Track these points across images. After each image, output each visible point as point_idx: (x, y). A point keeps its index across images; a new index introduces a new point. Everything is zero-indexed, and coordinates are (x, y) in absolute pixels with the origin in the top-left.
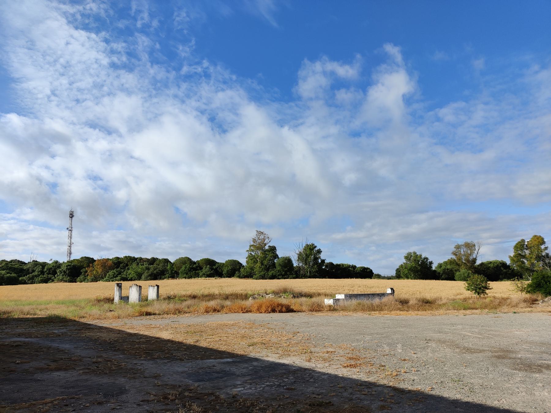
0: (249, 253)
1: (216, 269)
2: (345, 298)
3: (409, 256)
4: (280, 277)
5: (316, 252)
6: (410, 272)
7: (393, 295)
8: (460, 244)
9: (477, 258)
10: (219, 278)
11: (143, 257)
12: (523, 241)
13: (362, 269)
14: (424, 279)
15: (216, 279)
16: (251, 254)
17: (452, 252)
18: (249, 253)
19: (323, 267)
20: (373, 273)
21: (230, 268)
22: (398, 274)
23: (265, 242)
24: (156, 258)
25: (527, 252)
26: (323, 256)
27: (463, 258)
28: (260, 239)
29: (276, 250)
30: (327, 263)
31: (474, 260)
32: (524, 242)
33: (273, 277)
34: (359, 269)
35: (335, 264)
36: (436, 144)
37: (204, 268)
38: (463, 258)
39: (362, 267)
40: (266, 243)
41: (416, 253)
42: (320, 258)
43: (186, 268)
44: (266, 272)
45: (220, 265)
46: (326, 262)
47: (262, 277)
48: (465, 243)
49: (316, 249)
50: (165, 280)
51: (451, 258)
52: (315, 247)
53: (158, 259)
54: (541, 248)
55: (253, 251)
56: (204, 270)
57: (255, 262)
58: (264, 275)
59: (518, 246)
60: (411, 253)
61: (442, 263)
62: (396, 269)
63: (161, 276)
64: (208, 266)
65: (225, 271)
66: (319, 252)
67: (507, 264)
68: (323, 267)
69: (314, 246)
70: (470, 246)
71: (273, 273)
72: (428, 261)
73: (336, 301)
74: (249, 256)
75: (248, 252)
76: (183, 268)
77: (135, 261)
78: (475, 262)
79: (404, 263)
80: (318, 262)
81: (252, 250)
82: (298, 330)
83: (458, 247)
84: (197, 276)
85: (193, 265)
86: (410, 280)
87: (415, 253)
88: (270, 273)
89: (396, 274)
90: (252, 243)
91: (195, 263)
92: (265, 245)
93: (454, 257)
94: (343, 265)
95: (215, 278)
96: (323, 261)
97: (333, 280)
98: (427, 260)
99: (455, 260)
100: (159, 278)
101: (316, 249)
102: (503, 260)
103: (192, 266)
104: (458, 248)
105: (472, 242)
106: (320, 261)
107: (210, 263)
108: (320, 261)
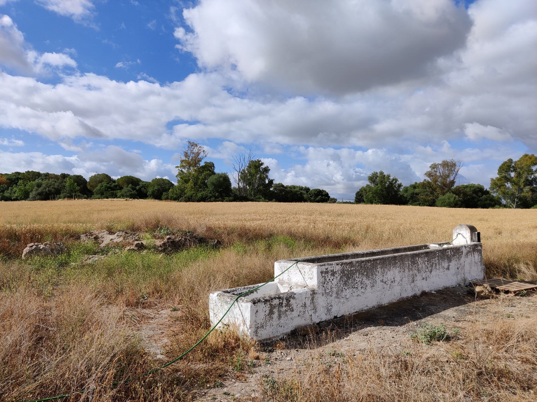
0: (179, 170)
1: (140, 189)
2: (323, 283)
3: (374, 177)
4: (212, 199)
5: (262, 170)
6: (375, 195)
7: (480, 252)
8: (437, 163)
9: (455, 180)
10: (131, 199)
11: (50, 173)
13: (316, 192)
14: (397, 205)
15: (126, 200)
16: (181, 171)
17: (425, 172)
18: (179, 170)
19: (271, 189)
20: (329, 197)
21: (157, 188)
22: (358, 198)
23: (200, 156)
24: (67, 174)
25: (513, 174)
26: (271, 175)
27: (440, 179)
28: (193, 153)
29: (214, 167)
30: (276, 184)
31: (453, 182)
32: (511, 163)
33: (203, 199)
34: (313, 192)
35: (285, 186)
36: (303, 194)
37: (125, 188)
38: (440, 179)
39: (316, 190)
40: (201, 158)
41: (383, 173)
42: (267, 177)
43: (101, 187)
44: (194, 193)
45: (145, 184)
46: (274, 182)
47: (189, 198)
49: (263, 167)
50: (60, 200)
51: (425, 180)
52: (262, 164)
53: (69, 175)
54: (533, 170)
55: (184, 167)
56: (125, 189)
57: (187, 181)
58: (191, 196)
59: (505, 167)
60: (377, 173)
61: (408, 187)
63: (54, 195)
64: (130, 185)
65: (150, 191)
66: (267, 170)
67: (484, 188)
68: (271, 189)
69: (260, 163)
70: (450, 166)
71: (203, 194)
72: (398, 183)
73: (272, 307)
74: (180, 174)
75: (177, 169)
76: (98, 188)
77: (39, 177)
78: (453, 185)
80: (265, 182)
81: (183, 166)
83: (434, 167)
84: (114, 196)
85: (112, 184)
86: (374, 205)
87: (382, 173)
88: (199, 195)
89: (355, 198)
90: (184, 158)
91: (114, 181)
92: (200, 161)
93: (428, 179)
94: (294, 187)
95: (125, 199)
96: (271, 182)
97: (282, 203)
98: (396, 182)
99: (429, 182)
100: (51, 198)
101: (263, 167)
103: (110, 185)
104: (434, 168)
105: (453, 160)
106: (267, 182)
107: (133, 182)
108: (267, 182)
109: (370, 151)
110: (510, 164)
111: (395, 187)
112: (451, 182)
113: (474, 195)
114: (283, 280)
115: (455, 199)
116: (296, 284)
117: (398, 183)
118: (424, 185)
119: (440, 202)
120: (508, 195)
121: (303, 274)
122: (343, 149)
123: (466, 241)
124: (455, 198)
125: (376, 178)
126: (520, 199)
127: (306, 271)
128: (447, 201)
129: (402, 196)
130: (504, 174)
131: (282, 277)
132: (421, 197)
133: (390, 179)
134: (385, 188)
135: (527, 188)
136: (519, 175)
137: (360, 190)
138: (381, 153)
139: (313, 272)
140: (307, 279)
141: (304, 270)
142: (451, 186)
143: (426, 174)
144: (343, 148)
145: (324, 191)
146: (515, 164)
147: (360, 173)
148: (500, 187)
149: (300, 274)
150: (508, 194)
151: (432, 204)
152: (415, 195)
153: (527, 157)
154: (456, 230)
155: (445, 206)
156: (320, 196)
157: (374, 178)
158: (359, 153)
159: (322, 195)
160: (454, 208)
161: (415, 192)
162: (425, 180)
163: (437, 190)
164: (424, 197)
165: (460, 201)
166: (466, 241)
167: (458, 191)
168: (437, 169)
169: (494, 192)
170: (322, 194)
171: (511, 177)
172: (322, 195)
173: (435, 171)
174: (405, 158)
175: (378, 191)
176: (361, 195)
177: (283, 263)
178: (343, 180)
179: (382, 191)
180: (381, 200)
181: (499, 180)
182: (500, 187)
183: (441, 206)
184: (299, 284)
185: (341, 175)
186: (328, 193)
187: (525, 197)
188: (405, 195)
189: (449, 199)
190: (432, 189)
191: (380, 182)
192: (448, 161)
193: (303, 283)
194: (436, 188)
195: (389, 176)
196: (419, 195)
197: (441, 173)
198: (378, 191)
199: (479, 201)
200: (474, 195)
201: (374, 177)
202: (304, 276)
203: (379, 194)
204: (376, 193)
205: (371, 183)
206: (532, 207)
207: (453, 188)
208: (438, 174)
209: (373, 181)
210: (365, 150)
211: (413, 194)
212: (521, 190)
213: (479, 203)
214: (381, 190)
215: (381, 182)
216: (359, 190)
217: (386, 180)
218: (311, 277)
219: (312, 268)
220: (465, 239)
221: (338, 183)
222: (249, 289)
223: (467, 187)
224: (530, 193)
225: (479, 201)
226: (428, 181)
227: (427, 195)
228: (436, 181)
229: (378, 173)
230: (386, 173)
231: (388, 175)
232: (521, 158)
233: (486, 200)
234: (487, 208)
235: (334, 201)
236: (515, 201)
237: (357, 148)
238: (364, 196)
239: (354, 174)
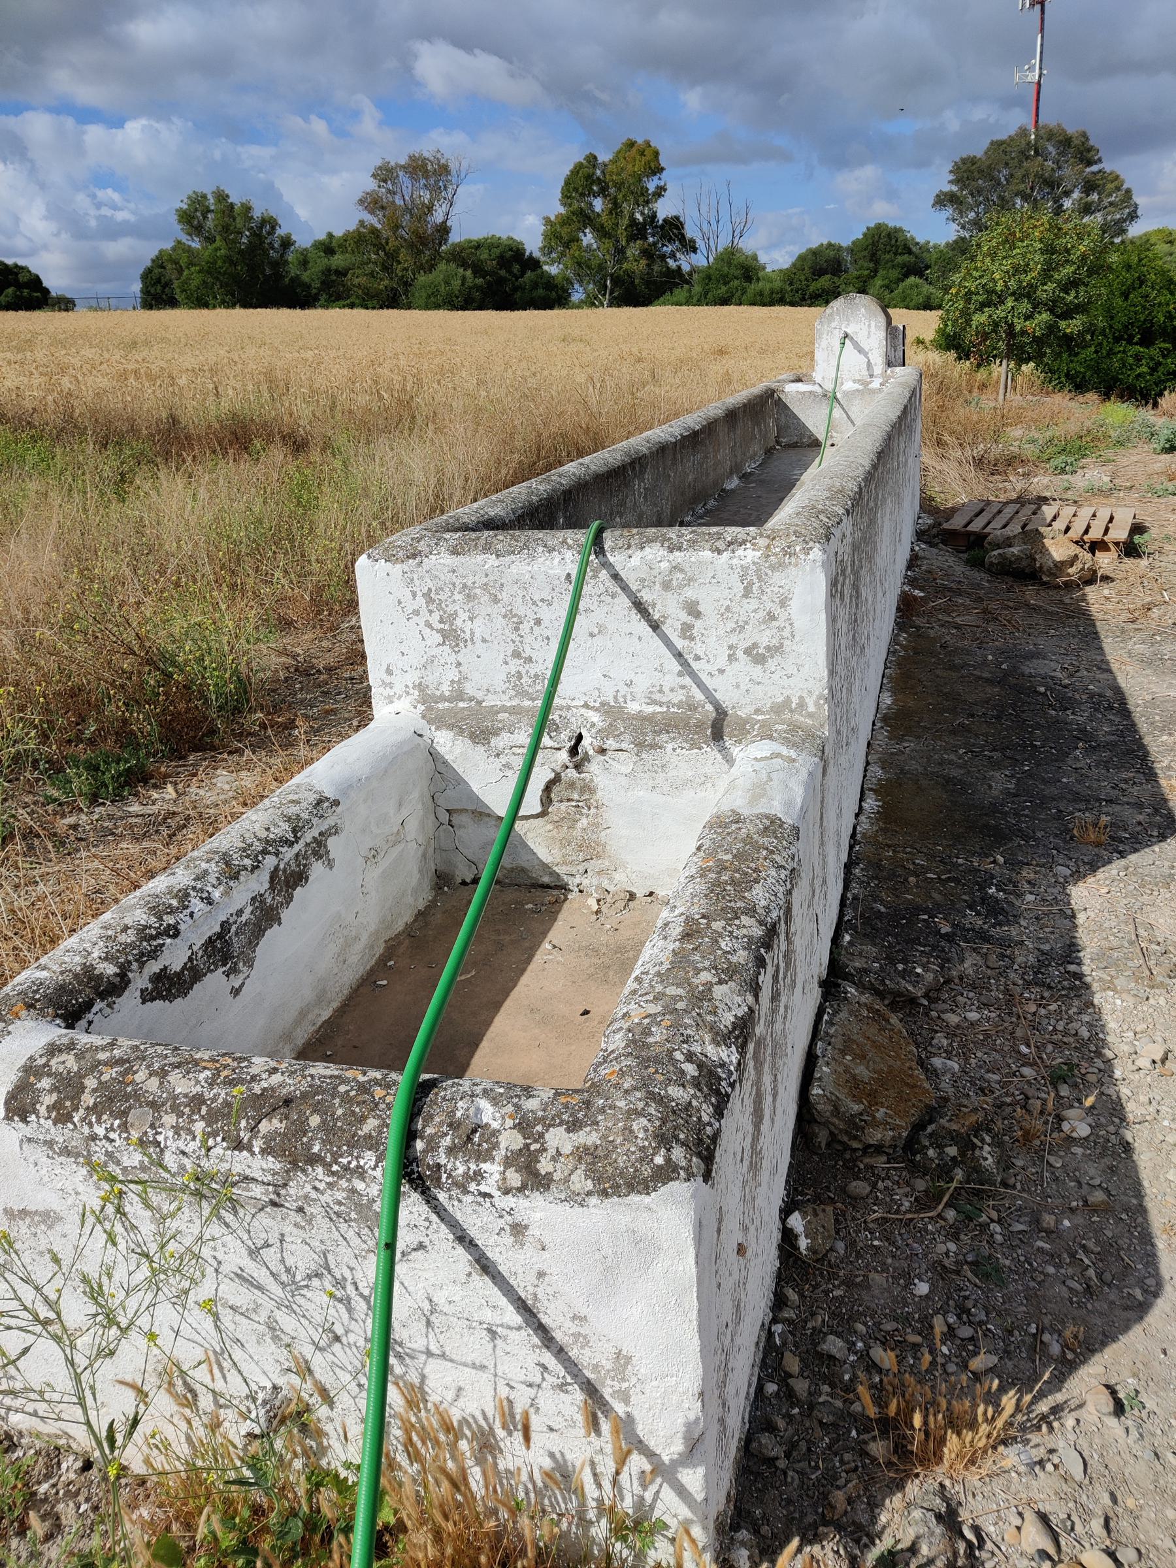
3: (196, 210)
6: (210, 280)
9: (449, 223)
12: (592, 159)
14: (295, 307)
17: (360, 195)
22: (153, 291)
25: (598, 204)
41: (227, 196)
48: (412, 158)
59: (580, 182)
60: (204, 196)
61: (306, 250)
62: (141, 271)
79: (660, 192)
82: (727, 1273)
83: (385, 174)
87: (221, 197)
93: (373, 220)
98: (273, 228)
99: (374, 232)
102: (515, 237)
104: (385, 181)
105: (438, 151)
109: (134, 129)
110: (591, 171)
111: (273, 248)
112: (438, 231)
113: (503, 273)
114: (460, 696)
115: (463, 284)
116: (612, 712)
117: (280, 232)
118: (362, 239)
119: (424, 295)
120: (589, 267)
121: (671, 630)
122: (29, 116)
123: (869, 364)
124: (464, 278)
125: (205, 217)
126: (616, 280)
127: (708, 598)
128: (442, 289)
129: (296, 280)
130: (576, 205)
131: (453, 674)
132: (356, 281)
133: (252, 218)
134: (241, 252)
135: (633, 250)
136: (615, 208)
137: (153, 261)
138: (171, 134)
139: (783, 603)
140: (722, 661)
141: (690, 593)
142: (440, 245)
143: (361, 201)
144: (34, 109)
145: (22, 268)
146: (603, 172)
147: (115, 208)
148: (567, 245)
149: (643, 628)
150: (589, 267)
151: (392, 300)
152: (334, 278)
153: (634, 150)
154: (830, 322)
155: (437, 307)
156: (10, 290)
157: (199, 214)
158: (94, 133)
159: (20, 286)
160: (460, 313)
161: (334, 267)
162: (362, 222)
163: (401, 257)
164: (362, 280)
165: (478, 288)
166: (869, 364)
167: (467, 255)
168: (394, 184)
169: (553, 262)
170: (17, 280)
171: (593, 211)
172: (20, 286)
173: (389, 191)
174: (253, 154)
175: (219, 263)
176: (159, 281)
177: (448, 560)
178: (57, 235)
179: (233, 263)
180: (233, 295)
181: (565, 221)
182: (567, 245)
183: (427, 307)
184: (633, 707)
185: (46, 218)
186: (37, 277)
187: (630, 274)
188: (305, 277)
189: (447, 283)
190: (386, 254)
191: (220, 228)
192: (426, 154)
193: (679, 696)
194: (397, 251)
195: (247, 208)
196: (349, 276)
197: (407, 198)
198: (219, 263)
199: (516, 289)
200: (503, 273)
201: (196, 210)
202: (680, 644)
203: (225, 273)
204: (210, 270)
205: (190, 235)
206: (656, 302)
207: (444, 248)
208: (399, 202)
209: (196, 228)
210: (117, 122)
211: (328, 271)
212: (620, 252)
213: (518, 295)
214: (228, 259)
215: (226, 229)
216: (149, 264)
217: (239, 222)
218: (765, 638)
219: (779, 566)
220: (862, 356)
221: (45, 247)
222: (270, 862)
223: (478, 246)
224: (643, 262)
225: (516, 289)
226: (372, 225)
227: (372, 275)
228: (397, 227)
229: (210, 197)
230: (235, 198)
231: (242, 205)
232: (619, 152)
233: (535, 285)
234: (551, 308)
235: (66, 304)
236: (606, 286)
237: (87, 115)
238: (176, 284)
239: (93, 212)
